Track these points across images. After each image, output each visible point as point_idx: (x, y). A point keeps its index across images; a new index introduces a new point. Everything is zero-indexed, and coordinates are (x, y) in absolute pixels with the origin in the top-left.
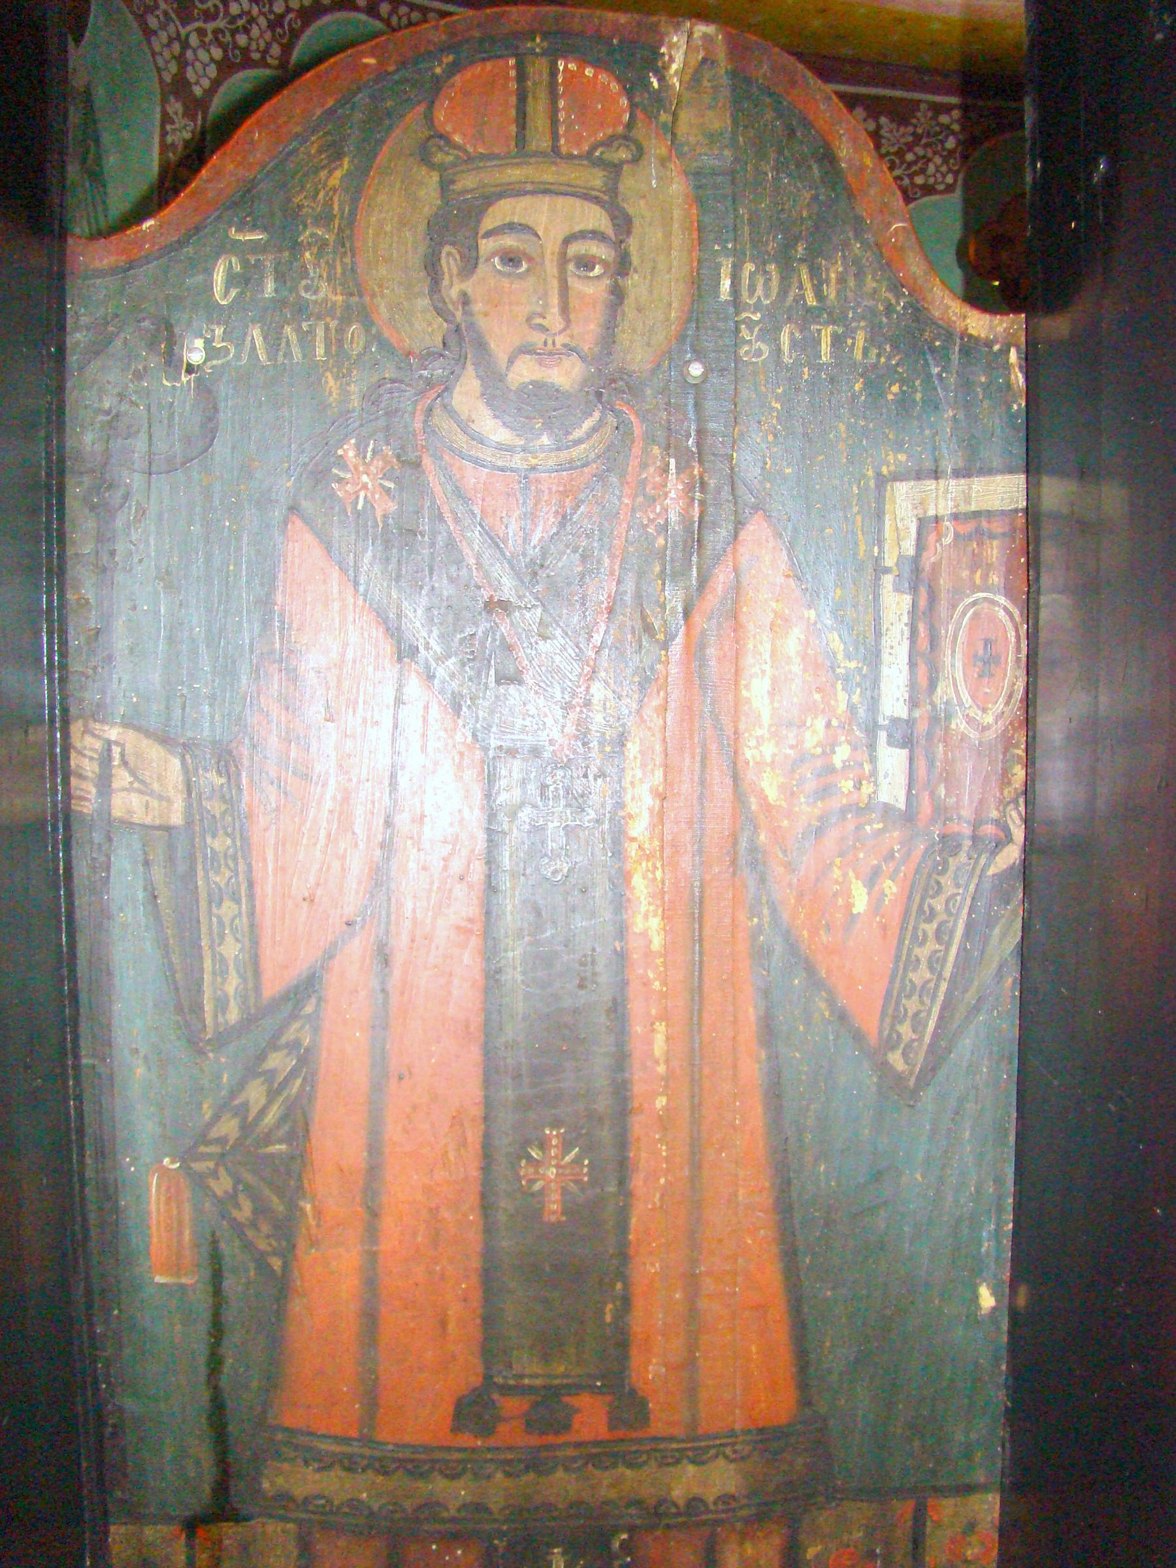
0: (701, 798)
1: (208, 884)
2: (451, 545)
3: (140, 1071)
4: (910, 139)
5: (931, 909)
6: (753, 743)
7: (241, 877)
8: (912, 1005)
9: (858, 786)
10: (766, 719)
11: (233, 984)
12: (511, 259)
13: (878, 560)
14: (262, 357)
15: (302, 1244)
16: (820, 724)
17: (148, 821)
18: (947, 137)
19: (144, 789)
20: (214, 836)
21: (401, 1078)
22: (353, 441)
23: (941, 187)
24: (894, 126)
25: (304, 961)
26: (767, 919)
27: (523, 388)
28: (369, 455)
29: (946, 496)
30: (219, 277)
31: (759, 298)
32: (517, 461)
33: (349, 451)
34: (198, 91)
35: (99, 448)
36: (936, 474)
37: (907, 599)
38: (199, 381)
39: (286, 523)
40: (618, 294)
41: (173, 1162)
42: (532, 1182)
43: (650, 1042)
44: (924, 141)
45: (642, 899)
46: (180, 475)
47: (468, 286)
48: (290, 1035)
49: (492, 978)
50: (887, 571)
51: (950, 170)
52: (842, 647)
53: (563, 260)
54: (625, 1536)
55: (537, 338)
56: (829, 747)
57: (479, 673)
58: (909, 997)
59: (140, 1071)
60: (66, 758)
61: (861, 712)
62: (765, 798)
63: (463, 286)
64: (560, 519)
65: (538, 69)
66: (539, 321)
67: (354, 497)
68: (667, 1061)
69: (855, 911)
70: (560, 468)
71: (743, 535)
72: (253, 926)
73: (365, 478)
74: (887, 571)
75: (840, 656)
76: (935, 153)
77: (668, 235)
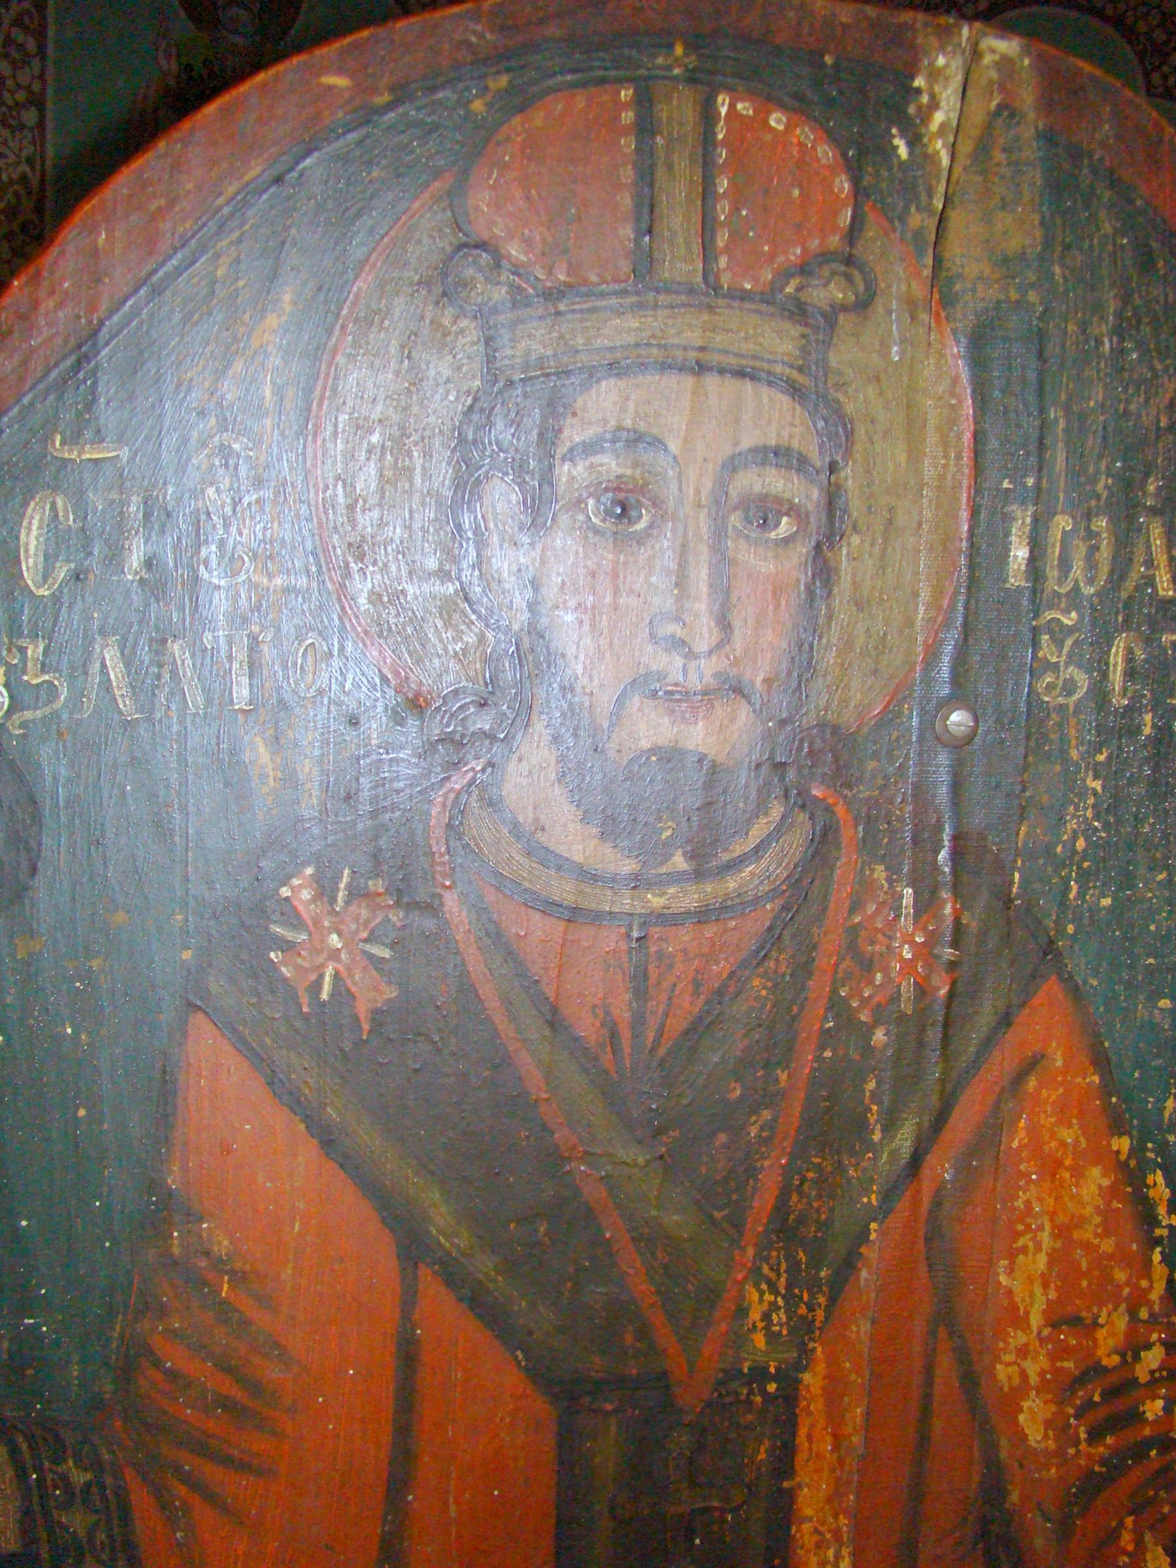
14: (125, 704)
28: (341, 896)
53: (720, 504)
65: (678, 109)
73: (334, 940)
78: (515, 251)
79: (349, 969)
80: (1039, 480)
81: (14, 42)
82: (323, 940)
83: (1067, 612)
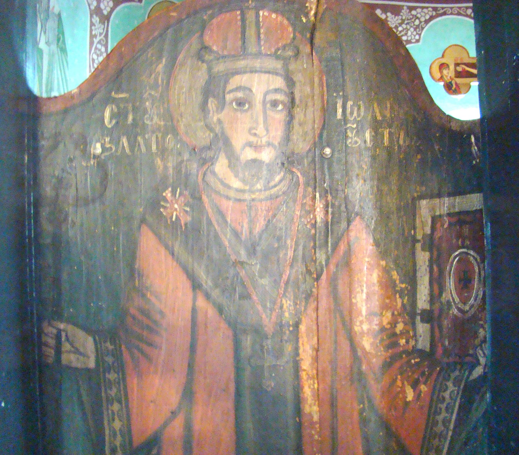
0: (336, 349)
2: (216, 236)
4: (400, 21)
6: (358, 324)
7: (122, 392)
8: (436, 442)
9: (407, 342)
10: (364, 313)
12: (240, 103)
13: (414, 237)
14: (127, 150)
16: (389, 314)
17: (79, 366)
18: (415, 20)
19: (77, 351)
22: (170, 189)
23: (414, 41)
24: (393, 16)
26: (366, 406)
27: (247, 162)
28: (177, 196)
29: (445, 205)
30: (107, 114)
32: (247, 196)
33: (168, 194)
34: (105, 13)
35: (53, 194)
36: (439, 196)
37: (427, 254)
38: (98, 164)
39: (140, 227)
40: (291, 117)
44: (406, 22)
45: (309, 398)
50: (418, 241)
51: (417, 34)
52: (398, 277)
53: (264, 103)
55: (253, 139)
57: (231, 296)
60: (40, 337)
61: (408, 308)
62: (365, 349)
63: (219, 116)
64: (266, 223)
65: (251, 16)
66: (254, 131)
69: (408, 400)
70: (267, 199)
71: (351, 227)
72: (128, 414)
73: (176, 206)
74: (418, 241)
75: (398, 282)
76: (411, 27)
77: (312, 89)
78: (215, 48)
79: (180, 213)
80: (343, 92)
83: (353, 124)
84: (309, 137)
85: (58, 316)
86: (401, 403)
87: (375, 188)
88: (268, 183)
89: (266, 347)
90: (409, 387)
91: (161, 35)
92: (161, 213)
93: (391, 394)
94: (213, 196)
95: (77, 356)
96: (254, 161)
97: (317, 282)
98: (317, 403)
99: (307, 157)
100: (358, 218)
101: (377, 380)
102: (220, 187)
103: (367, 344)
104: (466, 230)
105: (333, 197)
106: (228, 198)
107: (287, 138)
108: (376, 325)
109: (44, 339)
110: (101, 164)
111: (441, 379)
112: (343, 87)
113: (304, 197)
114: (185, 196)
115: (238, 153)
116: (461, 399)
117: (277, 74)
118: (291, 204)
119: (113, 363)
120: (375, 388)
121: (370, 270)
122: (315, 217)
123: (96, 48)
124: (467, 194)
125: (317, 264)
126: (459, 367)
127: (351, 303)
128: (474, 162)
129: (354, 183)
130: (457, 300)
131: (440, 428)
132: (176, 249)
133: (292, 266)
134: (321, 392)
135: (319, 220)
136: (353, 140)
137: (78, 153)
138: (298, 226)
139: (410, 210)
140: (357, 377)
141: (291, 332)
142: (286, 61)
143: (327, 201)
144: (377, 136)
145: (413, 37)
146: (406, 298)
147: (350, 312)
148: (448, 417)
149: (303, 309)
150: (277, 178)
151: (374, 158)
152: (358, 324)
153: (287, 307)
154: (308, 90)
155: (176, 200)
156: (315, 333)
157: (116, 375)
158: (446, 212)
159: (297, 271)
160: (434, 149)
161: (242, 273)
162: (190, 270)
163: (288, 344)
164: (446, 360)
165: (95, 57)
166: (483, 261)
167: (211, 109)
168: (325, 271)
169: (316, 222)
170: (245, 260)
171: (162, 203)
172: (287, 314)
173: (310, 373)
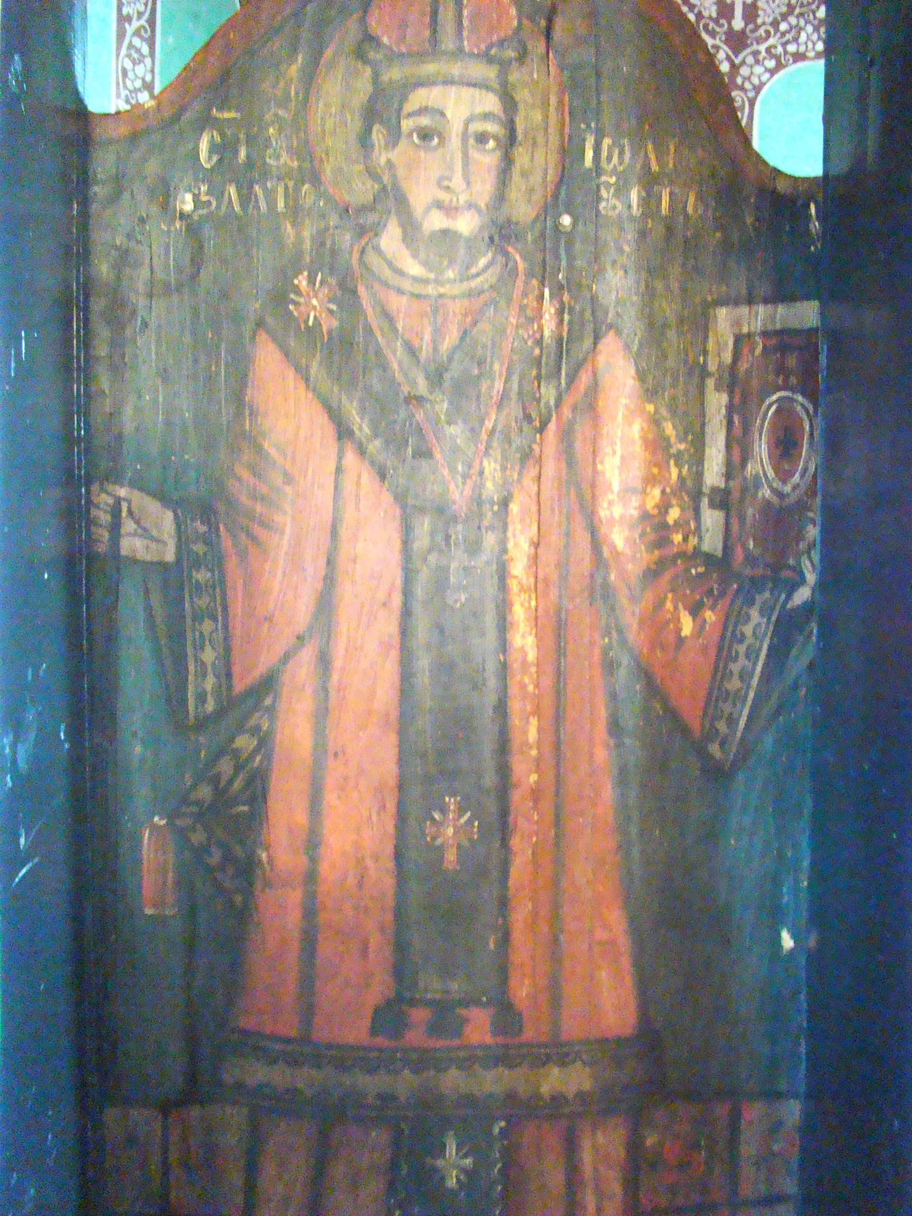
1: (192, 606)
2: (379, 353)
3: (139, 749)
4: (784, 9)
5: (743, 635)
6: (605, 505)
8: (727, 708)
9: (685, 539)
10: (616, 487)
11: (210, 683)
12: (425, 135)
13: (705, 366)
14: (237, 209)
15: (258, 885)
16: (657, 492)
17: (148, 558)
19: (145, 533)
20: (198, 571)
21: (336, 754)
22: (306, 273)
23: (811, 54)
25: (264, 663)
27: (433, 234)
28: (317, 284)
29: (759, 318)
31: (615, 165)
32: (431, 290)
33: (302, 281)
37: (724, 398)
39: (253, 337)
41: (161, 819)
42: (434, 839)
43: (525, 732)
44: (797, 11)
46: (175, 298)
47: (393, 155)
48: (252, 722)
49: (406, 675)
54: (503, 1124)
55: (444, 196)
56: (663, 507)
58: (725, 701)
59: (139, 749)
60: (88, 511)
61: (689, 483)
62: (615, 547)
63: (390, 156)
66: (446, 183)
67: (306, 317)
68: (538, 666)
71: (600, 347)
73: (315, 302)
78: (385, 40)
80: (597, 124)
81: (134, 47)
82: (310, 302)
83: (611, 177)
84: (537, 197)
85: (114, 476)
86: (671, 638)
87: (643, 284)
88: (468, 268)
89: (453, 537)
90: (687, 613)
91: (295, 15)
92: (291, 313)
93: (657, 626)
94: (376, 286)
95: (145, 542)
96: (445, 233)
97: (541, 434)
98: (534, 632)
99: (532, 229)
100: (612, 333)
101: (632, 599)
102: (387, 273)
103: (618, 538)
104: (792, 361)
105: (571, 298)
106: (400, 292)
107: (500, 197)
108: (635, 508)
109: (94, 512)
110: (193, 228)
111: (739, 602)
112: (598, 112)
113: (525, 294)
114: (330, 285)
115: (419, 219)
116: (771, 639)
117: (488, 88)
118: (502, 303)
119: (205, 554)
120: (630, 615)
121: (629, 422)
122: (541, 328)
123: (131, 46)
124: (796, 301)
125: (542, 404)
126: (770, 585)
127: (595, 472)
128: (812, 248)
129: (609, 273)
130: (771, 473)
131: (734, 684)
132: (313, 371)
133: (500, 405)
134: (541, 612)
135: (547, 333)
136: (609, 204)
137: (154, 209)
138: (513, 343)
139: (700, 324)
140: (601, 592)
141: (495, 514)
142: (505, 66)
143: (562, 303)
144: (649, 200)
145: (810, 45)
146: (686, 467)
147: (593, 485)
148: (751, 666)
149: (516, 476)
150: (482, 262)
151: (643, 234)
152: (605, 505)
153: (490, 473)
154: (538, 116)
155: (314, 290)
156: (535, 517)
157: (209, 575)
158: (759, 331)
159: (509, 414)
160: (744, 223)
161: (420, 416)
162: (335, 405)
163: (490, 533)
164: (748, 571)
165: (128, 64)
166: (816, 412)
167: (376, 141)
168: (554, 415)
169: (542, 336)
170: (424, 394)
171: (292, 296)
172: (489, 485)
173: (524, 581)
